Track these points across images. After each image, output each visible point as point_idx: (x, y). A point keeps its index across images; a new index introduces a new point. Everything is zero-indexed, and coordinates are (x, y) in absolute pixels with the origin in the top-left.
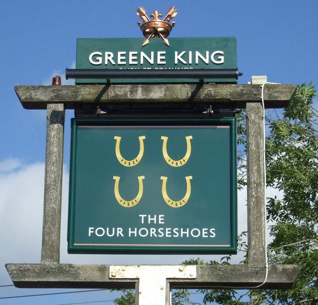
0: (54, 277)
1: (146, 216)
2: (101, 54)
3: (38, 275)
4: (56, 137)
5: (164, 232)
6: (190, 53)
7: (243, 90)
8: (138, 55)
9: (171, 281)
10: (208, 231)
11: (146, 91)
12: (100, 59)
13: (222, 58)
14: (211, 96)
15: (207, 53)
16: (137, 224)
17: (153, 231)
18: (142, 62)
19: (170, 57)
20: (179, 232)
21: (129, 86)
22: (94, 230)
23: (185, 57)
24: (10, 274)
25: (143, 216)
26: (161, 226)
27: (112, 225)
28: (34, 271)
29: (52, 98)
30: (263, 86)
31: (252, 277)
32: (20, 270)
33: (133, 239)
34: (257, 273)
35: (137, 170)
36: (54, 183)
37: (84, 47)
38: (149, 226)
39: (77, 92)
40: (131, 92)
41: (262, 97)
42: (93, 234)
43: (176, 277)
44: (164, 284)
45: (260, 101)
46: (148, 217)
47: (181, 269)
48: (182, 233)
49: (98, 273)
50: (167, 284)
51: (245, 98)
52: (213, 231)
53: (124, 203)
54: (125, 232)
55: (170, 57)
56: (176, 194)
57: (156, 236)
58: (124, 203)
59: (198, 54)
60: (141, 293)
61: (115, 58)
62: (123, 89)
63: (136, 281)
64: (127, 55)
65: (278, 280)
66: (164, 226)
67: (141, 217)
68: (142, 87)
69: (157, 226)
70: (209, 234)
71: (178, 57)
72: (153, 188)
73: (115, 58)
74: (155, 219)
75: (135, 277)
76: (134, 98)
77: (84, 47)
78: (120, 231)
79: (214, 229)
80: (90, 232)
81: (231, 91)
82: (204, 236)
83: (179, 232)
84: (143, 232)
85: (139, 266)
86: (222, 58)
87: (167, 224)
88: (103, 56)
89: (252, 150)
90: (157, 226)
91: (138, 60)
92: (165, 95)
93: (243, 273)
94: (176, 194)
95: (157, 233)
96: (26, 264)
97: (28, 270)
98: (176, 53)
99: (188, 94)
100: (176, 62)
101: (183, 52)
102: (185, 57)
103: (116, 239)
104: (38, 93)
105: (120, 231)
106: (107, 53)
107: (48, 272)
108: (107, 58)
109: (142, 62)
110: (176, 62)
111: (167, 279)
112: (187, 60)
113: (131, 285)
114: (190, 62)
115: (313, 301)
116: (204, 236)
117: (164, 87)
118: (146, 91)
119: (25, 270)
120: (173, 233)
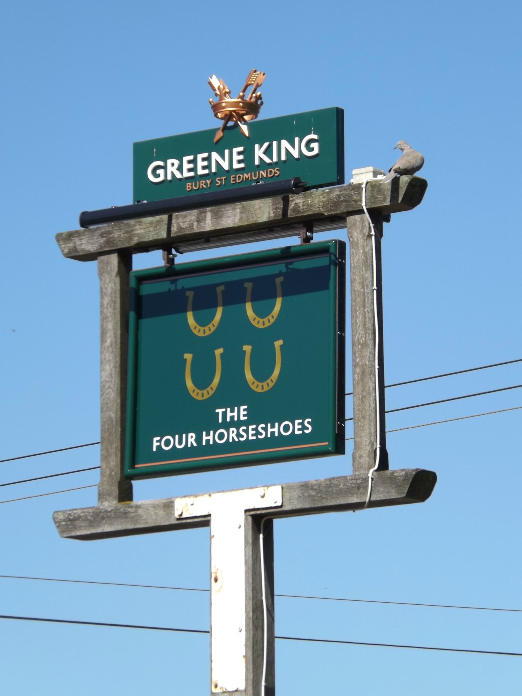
0: (111, 524)
1: (224, 410)
2: (161, 163)
4: (111, 306)
5: (246, 431)
6: (275, 144)
7: (339, 196)
9: (252, 513)
10: (302, 424)
11: (217, 216)
12: (161, 172)
13: (315, 145)
14: (299, 211)
15: (297, 140)
16: (213, 425)
17: (233, 433)
18: (214, 170)
19: (248, 154)
20: (265, 429)
22: (159, 441)
23: (268, 152)
24: (58, 527)
25: (220, 411)
26: (244, 423)
27: (179, 430)
28: (86, 519)
29: (101, 246)
30: (363, 186)
31: (352, 494)
32: (70, 520)
33: (215, 448)
34: (359, 488)
36: (110, 379)
37: (145, 153)
38: (226, 426)
39: (132, 231)
41: (364, 204)
42: (159, 447)
43: (256, 507)
45: (361, 212)
46: (226, 411)
47: (262, 495)
48: (270, 430)
50: (246, 519)
52: (308, 423)
53: (198, 394)
54: (199, 439)
56: (262, 372)
57: (236, 440)
58: (198, 394)
59: (285, 143)
60: (213, 536)
61: (180, 169)
62: (188, 219)
63: (208, 518)
64: (194, 161)
65: (386, 494)
66: (246, 423)
67: (218, 413)
68: (211, 211)
69: (237, 424)
70: (304, 428)
71: (259, 152)
72: (234, 364)
73: (180, 169)
74: (235, 414)
75: (206, 514)
76: (202, 230)
77: (145, 153)
79: (310, 420)
80: (155, 444)
81: (324, 200)
82: (297, 432)
83: (265, 429)
85: (210, 495)
86: (315, 145)
87: (254, 418)
89: (355, 291)
90: (237, 424)
91: (208, 167)
92: (241, 218)
93: (341, 490)
94: (262, 372)
95: (239, 435)
96: (76, 509)
97: (79, 517)
98: (257, 146)
99: (269, 213)
100: (257, 162)
101: (266, 145)
103: (188, 451)
104: (84, 242)
106: (169, 162)
107: (103, 518)
109: (214, 170)
110: (257, 162)
111: (246, 511)
112: (271, 158)
114: (275, 159)
116: (297, 432)
117: (239, 206)
118: (217, 216)
119: (75, 519)
120: (258, 433)
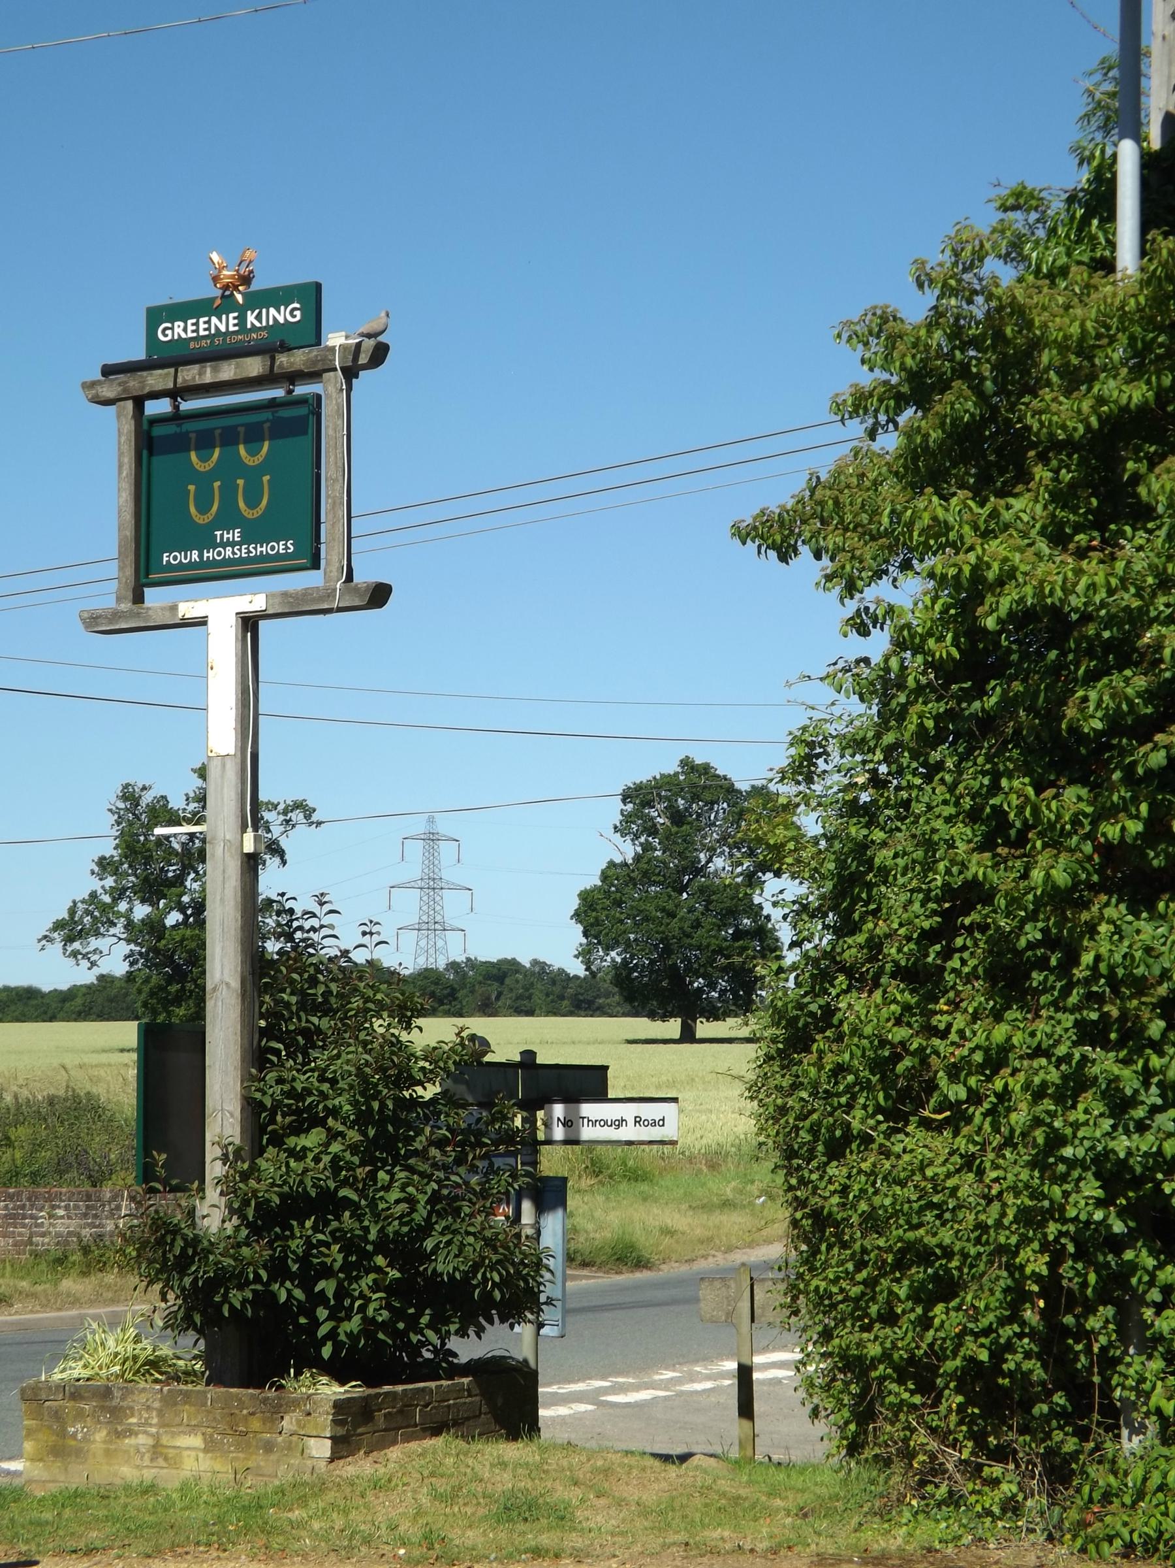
3: (111, 622)
8: (208, 322)
11: (215, 370)
13: (298, 313)
19: (242, 319)
21: (197, 366)
23: (259, 317)
33: (213, 563)
35: (261, 469)
37: (155, 316)
38: (224, 545)
40: (200, 374)
44: (232, 620)
45: (335, 369)
49: (167, 614)
51: (319, 367)
54: (201, 556)
55: (242, 319)
61: (185, 330)
64: (196, 324)
66: (240, 544)
69: (233, 544)
71: (251, 318)
73: (185, 330)
77: (155, 316)
78: (195, 555)
84: (219, 554)
87: (246, 540)
88: (172, 329)
90: (233, 544)
102: (259, 317)
103: (192, 565)
105: (195, 555)
108: (176, 330)
113: (202, 622)
115: (305, 1011)
118: (215, 370)
